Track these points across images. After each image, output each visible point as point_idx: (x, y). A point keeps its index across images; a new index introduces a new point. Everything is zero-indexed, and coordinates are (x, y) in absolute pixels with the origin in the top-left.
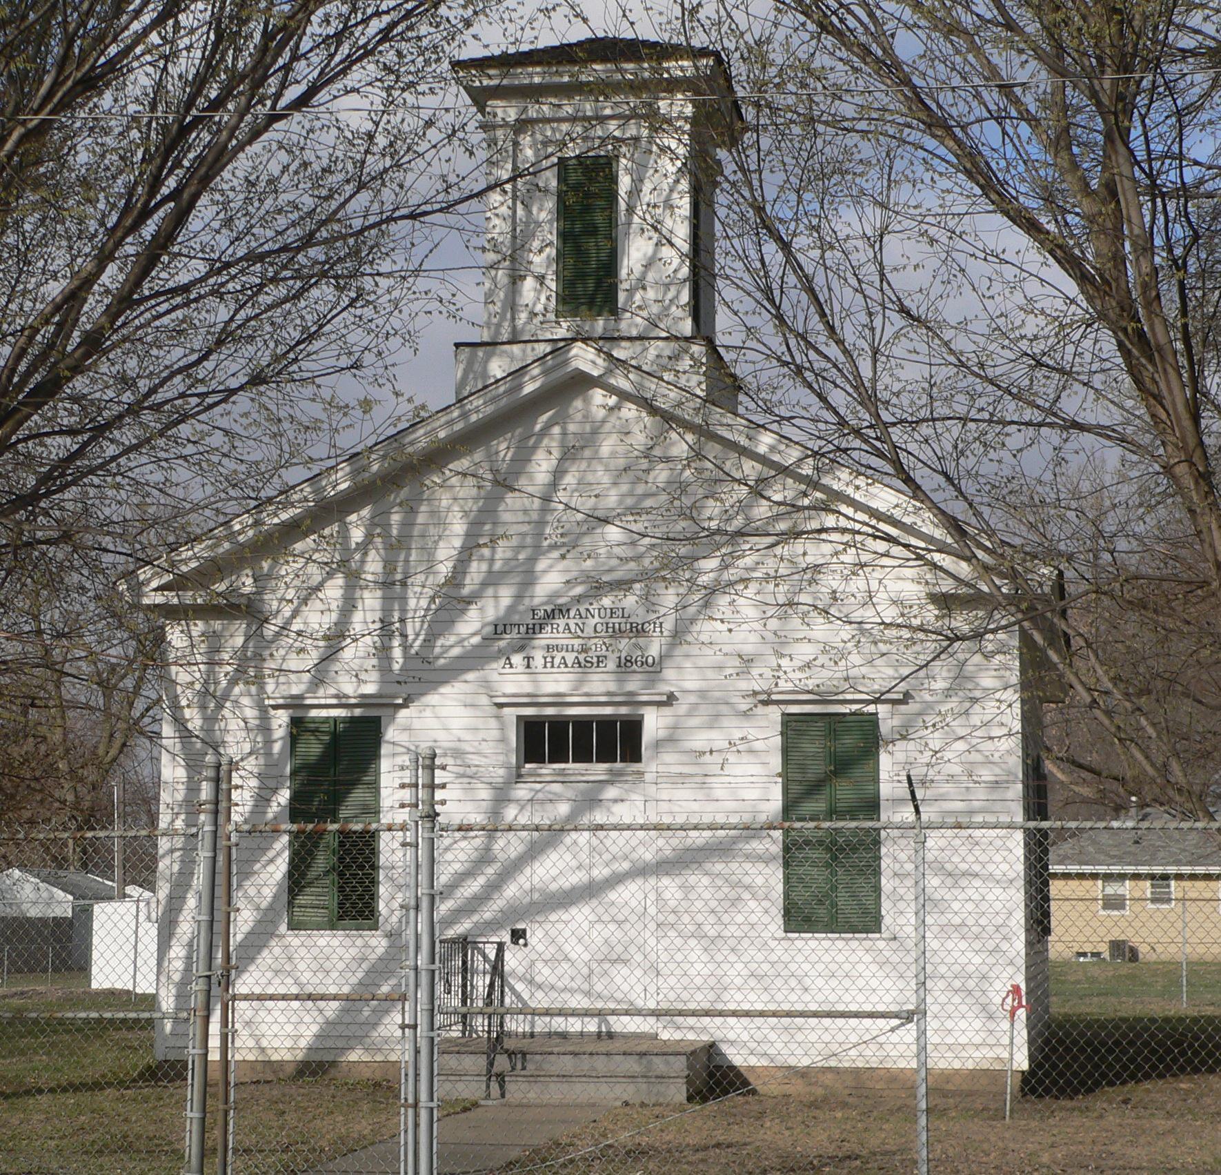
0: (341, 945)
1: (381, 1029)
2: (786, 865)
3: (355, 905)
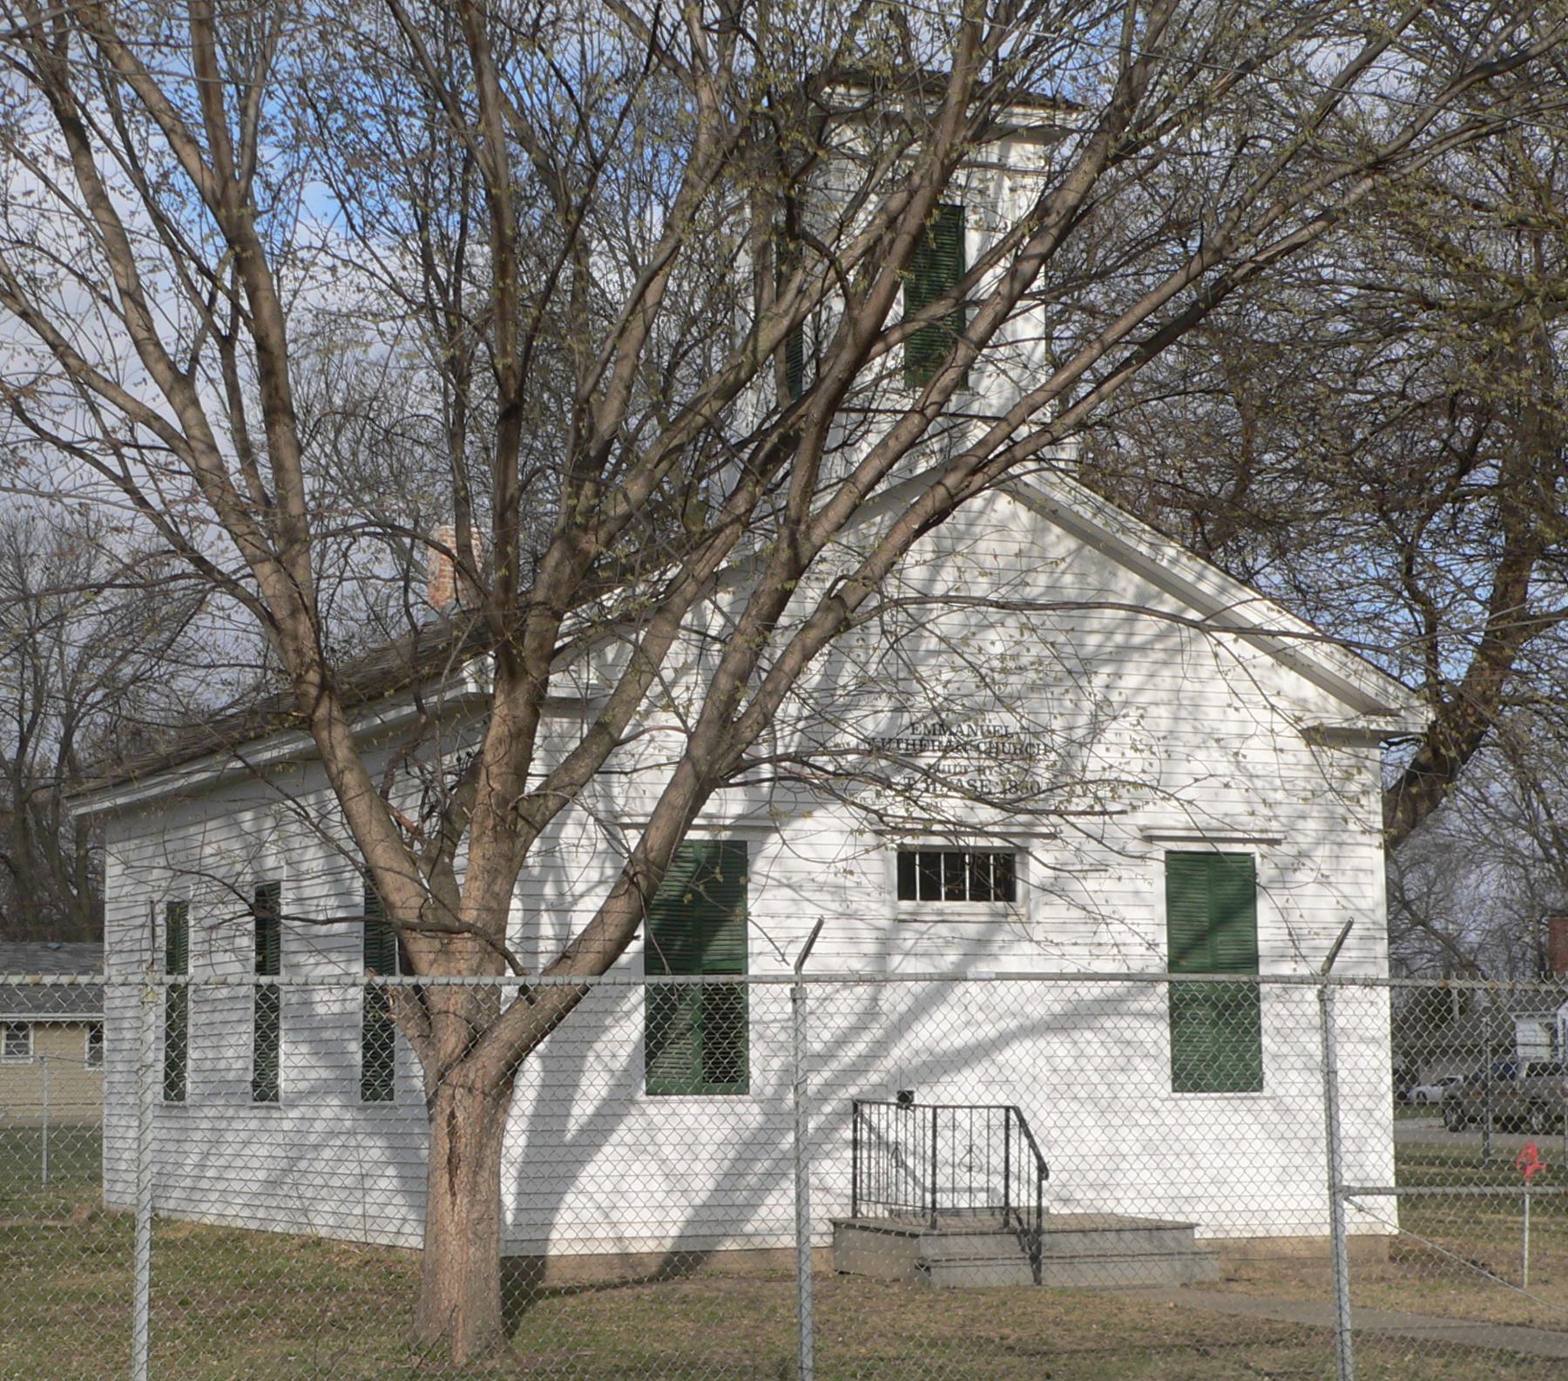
0: (718, 1113)
1: (763, 1211)
2: (1173, 1025)
3: (723, 1069)
